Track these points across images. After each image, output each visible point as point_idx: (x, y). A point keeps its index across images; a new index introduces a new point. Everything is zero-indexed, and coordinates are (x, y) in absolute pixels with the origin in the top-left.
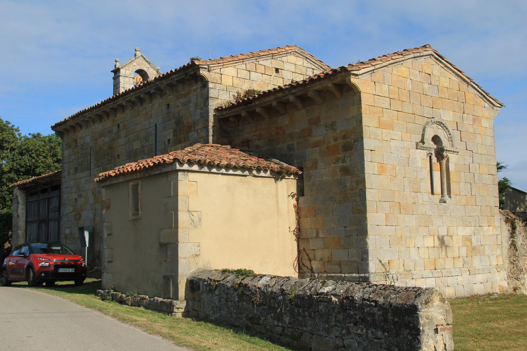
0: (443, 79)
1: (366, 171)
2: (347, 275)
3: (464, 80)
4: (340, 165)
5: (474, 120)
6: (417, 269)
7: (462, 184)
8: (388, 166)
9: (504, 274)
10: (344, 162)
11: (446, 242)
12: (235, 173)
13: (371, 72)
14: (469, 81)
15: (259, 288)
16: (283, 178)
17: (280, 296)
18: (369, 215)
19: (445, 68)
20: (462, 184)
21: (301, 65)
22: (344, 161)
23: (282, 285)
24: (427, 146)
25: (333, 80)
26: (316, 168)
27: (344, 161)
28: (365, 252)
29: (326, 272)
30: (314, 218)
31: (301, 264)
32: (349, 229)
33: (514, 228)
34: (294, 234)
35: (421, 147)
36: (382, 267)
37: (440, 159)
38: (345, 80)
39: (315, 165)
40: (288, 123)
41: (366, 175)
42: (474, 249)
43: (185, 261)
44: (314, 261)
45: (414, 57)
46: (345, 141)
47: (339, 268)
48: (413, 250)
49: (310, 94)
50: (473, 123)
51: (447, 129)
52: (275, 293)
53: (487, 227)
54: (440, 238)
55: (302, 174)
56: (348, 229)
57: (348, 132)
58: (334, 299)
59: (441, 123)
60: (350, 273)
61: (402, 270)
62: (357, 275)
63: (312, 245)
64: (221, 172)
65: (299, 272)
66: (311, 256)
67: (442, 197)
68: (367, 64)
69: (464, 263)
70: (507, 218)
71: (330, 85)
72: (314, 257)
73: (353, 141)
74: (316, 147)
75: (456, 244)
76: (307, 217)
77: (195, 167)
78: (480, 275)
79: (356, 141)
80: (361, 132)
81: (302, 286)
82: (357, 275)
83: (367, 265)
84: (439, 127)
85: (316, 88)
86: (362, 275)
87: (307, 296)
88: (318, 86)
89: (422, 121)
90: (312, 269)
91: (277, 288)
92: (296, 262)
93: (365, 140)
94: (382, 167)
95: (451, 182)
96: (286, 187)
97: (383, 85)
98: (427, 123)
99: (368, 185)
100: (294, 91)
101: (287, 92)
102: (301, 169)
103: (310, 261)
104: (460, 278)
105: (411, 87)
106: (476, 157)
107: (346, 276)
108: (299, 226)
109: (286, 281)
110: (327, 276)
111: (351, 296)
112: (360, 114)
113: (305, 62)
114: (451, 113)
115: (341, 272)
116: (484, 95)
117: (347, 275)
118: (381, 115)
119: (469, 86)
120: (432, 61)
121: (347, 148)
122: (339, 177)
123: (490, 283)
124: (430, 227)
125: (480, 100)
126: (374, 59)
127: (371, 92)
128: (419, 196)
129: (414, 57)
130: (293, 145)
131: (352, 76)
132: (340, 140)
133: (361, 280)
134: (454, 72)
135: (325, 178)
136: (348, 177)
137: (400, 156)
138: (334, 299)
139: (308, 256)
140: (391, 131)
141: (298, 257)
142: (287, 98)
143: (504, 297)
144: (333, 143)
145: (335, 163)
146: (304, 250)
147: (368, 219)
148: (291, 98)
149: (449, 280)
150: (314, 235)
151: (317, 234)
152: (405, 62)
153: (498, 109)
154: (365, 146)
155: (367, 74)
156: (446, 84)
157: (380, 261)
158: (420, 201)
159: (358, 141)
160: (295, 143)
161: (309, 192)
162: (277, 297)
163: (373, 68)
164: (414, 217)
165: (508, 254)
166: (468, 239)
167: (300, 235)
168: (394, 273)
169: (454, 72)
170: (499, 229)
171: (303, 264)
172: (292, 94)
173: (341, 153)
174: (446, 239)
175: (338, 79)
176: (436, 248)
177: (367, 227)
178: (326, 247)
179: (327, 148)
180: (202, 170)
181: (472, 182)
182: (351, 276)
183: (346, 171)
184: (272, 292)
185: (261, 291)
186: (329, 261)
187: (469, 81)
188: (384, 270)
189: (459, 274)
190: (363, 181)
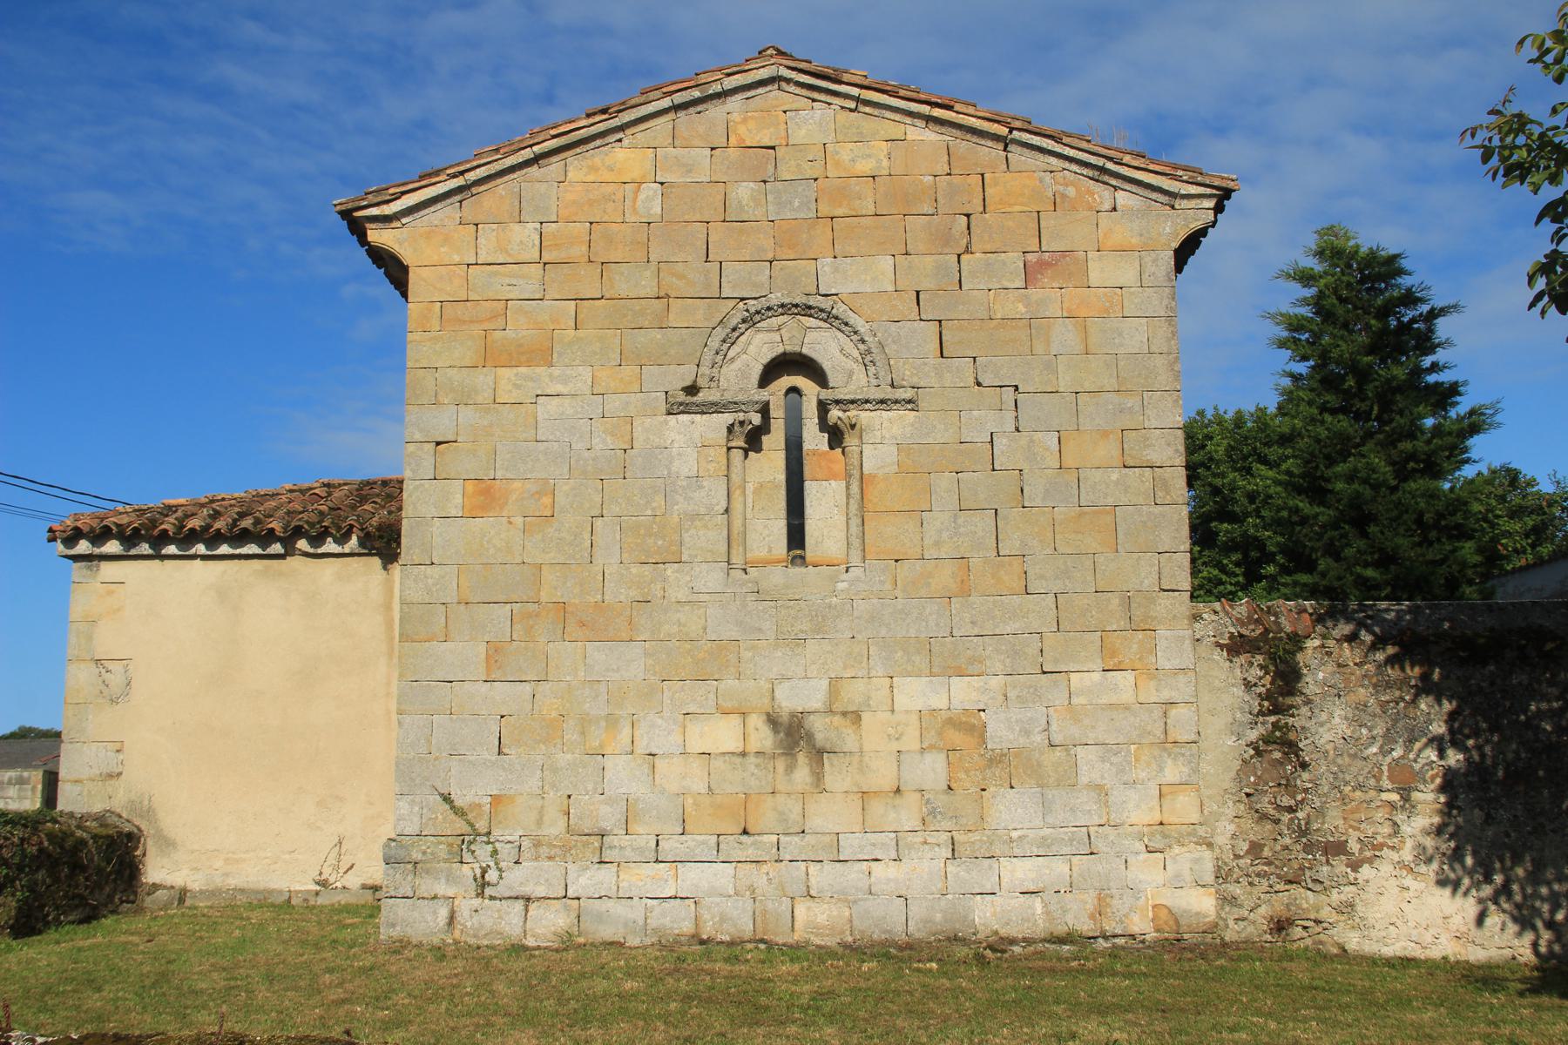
8: (517, 484)
9: (1194, 861)
12: (238, 551)
14: (1004, 131)
33: (1284, 683)
42: (996, 760)
43: (78, 788)
45: (677, 108)
51: (846, 324)
53: (1097, 676)
64: (192, 551)
77: (113, 547)
84: (811, 322)
94: (487, 492)
97: (516, 227)
127: (457, 259)
129: (677, 108)
134: (910, 114)
143: (1182, 964)
149: (821, 877)
157: (447, 799)
164: (636, 649)
176: (752, 759)
180: (133, 552)
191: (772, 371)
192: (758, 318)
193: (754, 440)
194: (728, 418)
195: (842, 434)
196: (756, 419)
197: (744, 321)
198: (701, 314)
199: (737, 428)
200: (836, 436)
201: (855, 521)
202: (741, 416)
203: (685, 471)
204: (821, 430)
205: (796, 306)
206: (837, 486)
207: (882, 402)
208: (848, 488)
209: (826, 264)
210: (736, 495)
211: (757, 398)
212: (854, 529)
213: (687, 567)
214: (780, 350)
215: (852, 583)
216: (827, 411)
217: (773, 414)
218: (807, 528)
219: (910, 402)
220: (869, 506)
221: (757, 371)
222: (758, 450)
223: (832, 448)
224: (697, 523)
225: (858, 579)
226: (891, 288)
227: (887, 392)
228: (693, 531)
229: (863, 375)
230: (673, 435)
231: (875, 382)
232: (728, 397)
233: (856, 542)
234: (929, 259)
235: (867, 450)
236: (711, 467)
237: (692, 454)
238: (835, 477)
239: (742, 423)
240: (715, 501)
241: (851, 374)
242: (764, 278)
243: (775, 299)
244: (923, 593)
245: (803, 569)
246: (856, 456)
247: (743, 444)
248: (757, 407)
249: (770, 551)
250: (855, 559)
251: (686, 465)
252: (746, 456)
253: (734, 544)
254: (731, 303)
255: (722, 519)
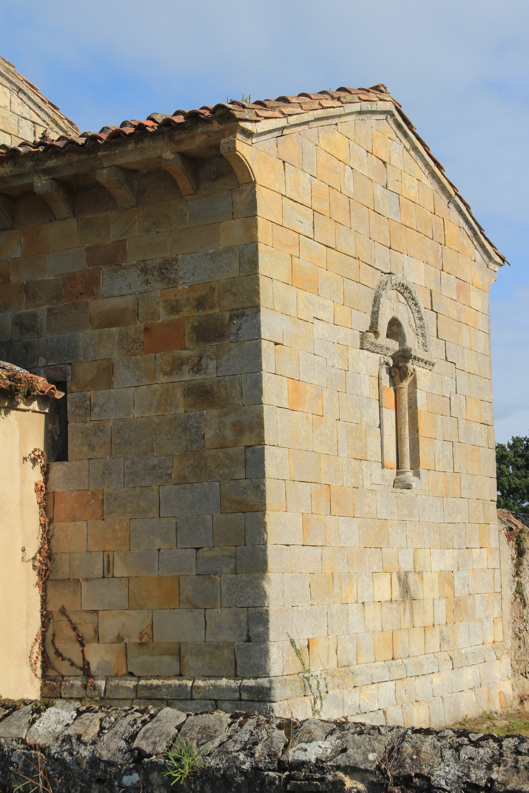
0: (408, 181)
1: (266, 399)
2: (200, 683)
3: (443, 189)
4: (187, 377)
5: (459, 289)
6: (362, 660)
7: (439, 443)
10: (198, 371)
11: (412, 588)
13: (277, 134)
14: (453, 194)
15: (43, 750)
16: (13, 407)
17: (129, 772)
18: (271, 517)
19: (412, 153)
20: (439, 443)
21: (5, 107)
22: (197, 368)
23: (133, 737)
24: (382, 343)
25: (180, 142)
26: (110, 385)
27: (197, 368)
28: (260, 618)
29: (131, 674)
30: (100, 523)
31: (51, 652)
32: (210, 554)
34: (34, 567)
35: (372, 344)
36: (296, 658)
37: (397, 378)
38: (217, 147)
39: (106, 374)
40: (18, 254)
41: (265, 407)
42: (458, 603)
44: (95, 645)
45: (360, 113)
46: (202, 313)
47: (177, 664)
48: (354, 609)
49: (103, 176)
50: (458, 297)
51: (416, 305)
52: (110, 763)
53: (478, 550)
54: (402, 577)
55: (65, 398)
56: (205, 553)
57: (213, 289)
58: (349, 783)
59: (407, 288)
60: (209, 677)
61: (333, 665)
62: (233, 683)
63: (88, 597)
65: (44, 677)
66: (87, 631)
67: (398, 474)
68: (273, 109)
69: (443, 639)
70: (511, 529)
71: (168, 155)
72: (96, 632)
73: (227, 315)
74: (110, 325)
75: (427, 589)
76: (74, 519)
78: (470, 670)
79: (238, 314)
80: (254, 292)
81: (211, 738)
82: (233, 683)
83: (265, 653)
85: (122, 161)
86: (250, 683)
87: (243, 773)
88: (130, 156)
89: (373, 279)
90: (86, 670)
91: (113, 746)
92: (36, 649)
93: (265, 316)
95: (420, 439)
96: (17, 433)
97: (301, 173)
98: (382, 286)
99: (268, 437)
100: (51, 163)
101: (30, 164)
102: (61, 385)
103: (82, 645)
104: (437, 680)
105: (352, 189)
106: (462, 377)
107: (198, 687)
108: (49, 542)
109: (144, 722)
110: (136, 687)
111: (417, 775)
112: (254, 243)
113: (16, 100)
114: (422, 265)
115: (180, 675)
116: (476, 232)
117: (200, 683)
118: (295, 253)
119: (451, 206)
120: (388, 128)
121: (210, 333)
122: (181, 410)
123: (484, 689)
124: (385, 550)
125: (467, 242)
126: (284, 100)
128: (365, 470)
129: (360, 113)
130: (34, 316)
131: (239, 136)
132: (186, 312)
133: (245, 696)
134: (427, 165)
135: (135, 413)
136: (211, 414)
137: (330, 363)
138: (349, 783)
139: (74, 629)
140: (315, 296)
141: (44, 634)
142: (26, 181)
144: (163, 317)
145: (169, 373)
146: (63, 611)
147: (270, 528)
148: (41, 183)
150: (98, 569)
151: (108, 566)
152: (343, 119)
153: (497, 268)
154: (265, 333)
155: (269, 136)
156: (413, 194)
157: (292, 642)
158: (367, 484)
159: (243, 315)
160: (42, 311)
161: (85, 449)
162: (119, 776)
163: (282, 122)
165: (511, 614)
166: (447, 579)
167: (49, 569)
168: (318, 673)
169: (427, 165)
170: (497, 554)
171: (58, 654)
172: (46, 172)
173: (187, 344)
174: (412, 579)
175: (196, 142)
177: (265, 551)
178: (134, 603)
179: (146, 330)
181: (455, 440)
182: (215, 687)
183: (202, 395)
184: (95, 761)
185: (49, 756)
186: (142, 645)
187: (453, 194)
188: (300, 668)
189: (435, 670)
190: (258, 425)
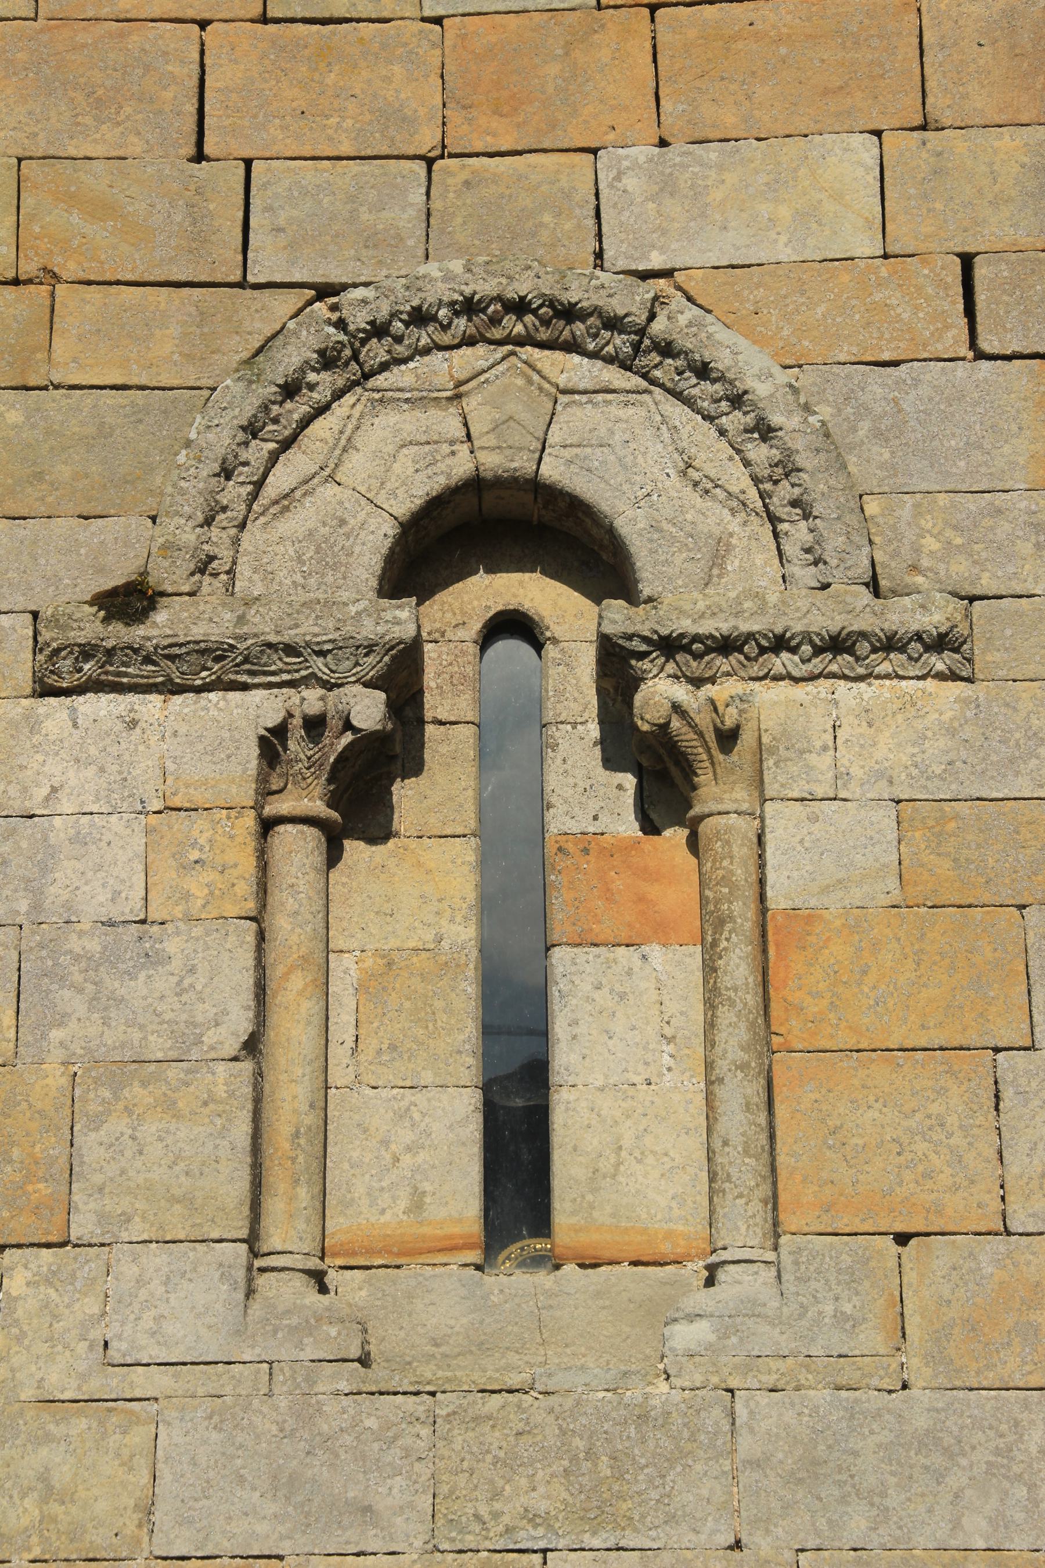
51: (703, 371)
84: (574, 370)
191: (434, 546)
192: (377, 351)
193: (363, 789)
194: (264, 707)
195: (687, 769)
196: (368, 709)
197: (327, 360)
198: (165, 338)
199: (296, 745)
200: (662, 774)
201: (739, 1093)
202: (312, 700)
203: (96, 901)
204: (610, 763)
205: (520, 307)
206: (670, 969)
207: (837, 644)
208: (710, 968)
209: (631, 169)
210: (293, 998)
211: (368, 630)
212: (738, 1120)
213: (92, 1261)
214: (460, 466)
215: (729, 1324)
216: (634, 683)
217: (434, 705)
218: (558, 1119)
219: (941, 643)
220: (791, 1028)
221: (375, 539)
222: (379, 831)
223: (650, 827)
224: (135, 1092)
225: (751, 1309)
226: (868, 245)
227: (854, 611)
228: (117, 1125)
229: (764, 557)
230: (55, 769)
231: (808, 575)
232: (264, 625)
233: (743, 1170)
234: (1007, 140)
235: (783, 824)
236: (197, 884)
237: (124, 840)
238: (662, 932)
239: (315, 725)
240: (203, 1012)
241: (719, 552)
242: (405, 215)
243: (442, 279)
244: (1012, 1366)
245: (543, 1278)
246: (743, 851)
247: (319, 807)
248: (372, 665)
249: (417, 1205)
250: (742, 1230)
251: (102, 874)
252: (333, 856)
253: (277, 1178)
254: (287, 302)
255: (231, 1080)
